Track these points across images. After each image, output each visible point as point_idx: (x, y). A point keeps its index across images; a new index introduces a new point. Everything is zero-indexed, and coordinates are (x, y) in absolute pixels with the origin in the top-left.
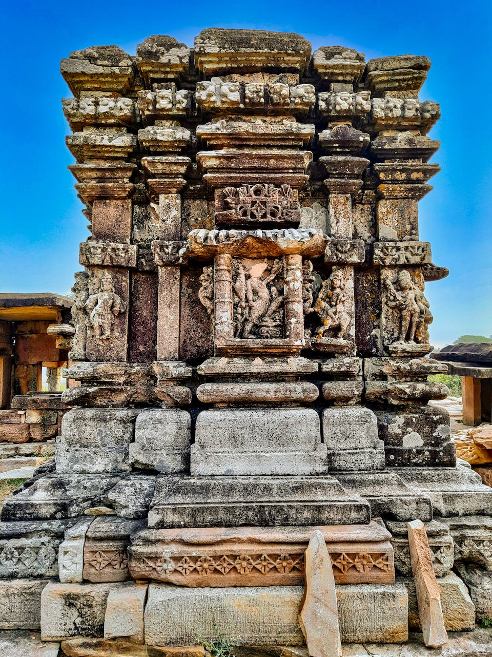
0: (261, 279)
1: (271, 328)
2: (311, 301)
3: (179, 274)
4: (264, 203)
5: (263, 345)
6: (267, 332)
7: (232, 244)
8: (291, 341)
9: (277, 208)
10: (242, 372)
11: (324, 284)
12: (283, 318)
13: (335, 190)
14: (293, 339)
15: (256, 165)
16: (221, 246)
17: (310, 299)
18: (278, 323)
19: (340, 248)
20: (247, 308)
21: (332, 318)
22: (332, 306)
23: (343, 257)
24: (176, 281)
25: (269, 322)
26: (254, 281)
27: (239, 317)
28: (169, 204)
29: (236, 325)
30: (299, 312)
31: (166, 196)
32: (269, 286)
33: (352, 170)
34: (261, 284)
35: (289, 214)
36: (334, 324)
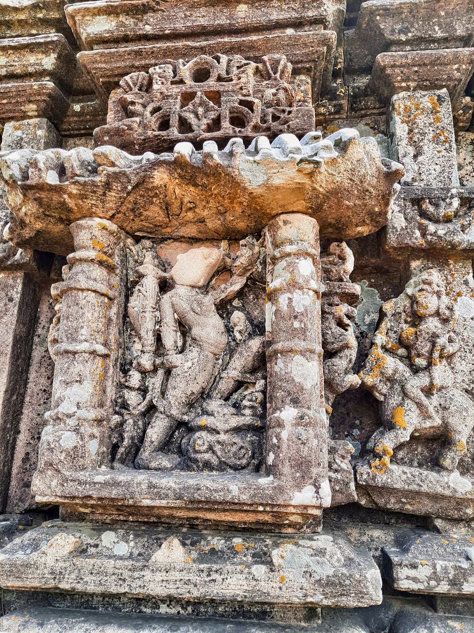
0: (206, 288)
1: (223, 437)
2: (353, 353)
3: (20, 288)
4: (215, 96)
5: (180, 498)
6: (211, 449)
7: (108, 186)
8: (280, 489)
9: (250, 105)
10: (114, 590)
11: (388, 307)
12: (263, 404)
13: (407, 79)
14: (286, 481)
15: (202, 22)
16: (74, 190)
17: (347, 346)
18: (247, 418)
19: (431, 209)
20: (161, 372)
21: (419, 405)
22: (415, 370)
23: (441, 232)
24: (11, 305)
25: (221, 416)
26: (181, 295)
27: (132, 398)
28: (22, 139)
29: (122, 424)
30: (308, 385)
31: (17, 124)
32: (223, 308)
33: (450, 27)
34: (200, 304)
35: (282, 116)
36: (428, 424)
